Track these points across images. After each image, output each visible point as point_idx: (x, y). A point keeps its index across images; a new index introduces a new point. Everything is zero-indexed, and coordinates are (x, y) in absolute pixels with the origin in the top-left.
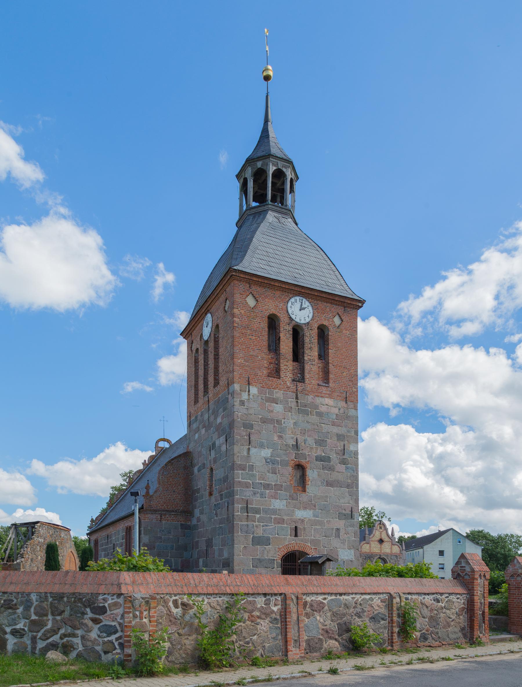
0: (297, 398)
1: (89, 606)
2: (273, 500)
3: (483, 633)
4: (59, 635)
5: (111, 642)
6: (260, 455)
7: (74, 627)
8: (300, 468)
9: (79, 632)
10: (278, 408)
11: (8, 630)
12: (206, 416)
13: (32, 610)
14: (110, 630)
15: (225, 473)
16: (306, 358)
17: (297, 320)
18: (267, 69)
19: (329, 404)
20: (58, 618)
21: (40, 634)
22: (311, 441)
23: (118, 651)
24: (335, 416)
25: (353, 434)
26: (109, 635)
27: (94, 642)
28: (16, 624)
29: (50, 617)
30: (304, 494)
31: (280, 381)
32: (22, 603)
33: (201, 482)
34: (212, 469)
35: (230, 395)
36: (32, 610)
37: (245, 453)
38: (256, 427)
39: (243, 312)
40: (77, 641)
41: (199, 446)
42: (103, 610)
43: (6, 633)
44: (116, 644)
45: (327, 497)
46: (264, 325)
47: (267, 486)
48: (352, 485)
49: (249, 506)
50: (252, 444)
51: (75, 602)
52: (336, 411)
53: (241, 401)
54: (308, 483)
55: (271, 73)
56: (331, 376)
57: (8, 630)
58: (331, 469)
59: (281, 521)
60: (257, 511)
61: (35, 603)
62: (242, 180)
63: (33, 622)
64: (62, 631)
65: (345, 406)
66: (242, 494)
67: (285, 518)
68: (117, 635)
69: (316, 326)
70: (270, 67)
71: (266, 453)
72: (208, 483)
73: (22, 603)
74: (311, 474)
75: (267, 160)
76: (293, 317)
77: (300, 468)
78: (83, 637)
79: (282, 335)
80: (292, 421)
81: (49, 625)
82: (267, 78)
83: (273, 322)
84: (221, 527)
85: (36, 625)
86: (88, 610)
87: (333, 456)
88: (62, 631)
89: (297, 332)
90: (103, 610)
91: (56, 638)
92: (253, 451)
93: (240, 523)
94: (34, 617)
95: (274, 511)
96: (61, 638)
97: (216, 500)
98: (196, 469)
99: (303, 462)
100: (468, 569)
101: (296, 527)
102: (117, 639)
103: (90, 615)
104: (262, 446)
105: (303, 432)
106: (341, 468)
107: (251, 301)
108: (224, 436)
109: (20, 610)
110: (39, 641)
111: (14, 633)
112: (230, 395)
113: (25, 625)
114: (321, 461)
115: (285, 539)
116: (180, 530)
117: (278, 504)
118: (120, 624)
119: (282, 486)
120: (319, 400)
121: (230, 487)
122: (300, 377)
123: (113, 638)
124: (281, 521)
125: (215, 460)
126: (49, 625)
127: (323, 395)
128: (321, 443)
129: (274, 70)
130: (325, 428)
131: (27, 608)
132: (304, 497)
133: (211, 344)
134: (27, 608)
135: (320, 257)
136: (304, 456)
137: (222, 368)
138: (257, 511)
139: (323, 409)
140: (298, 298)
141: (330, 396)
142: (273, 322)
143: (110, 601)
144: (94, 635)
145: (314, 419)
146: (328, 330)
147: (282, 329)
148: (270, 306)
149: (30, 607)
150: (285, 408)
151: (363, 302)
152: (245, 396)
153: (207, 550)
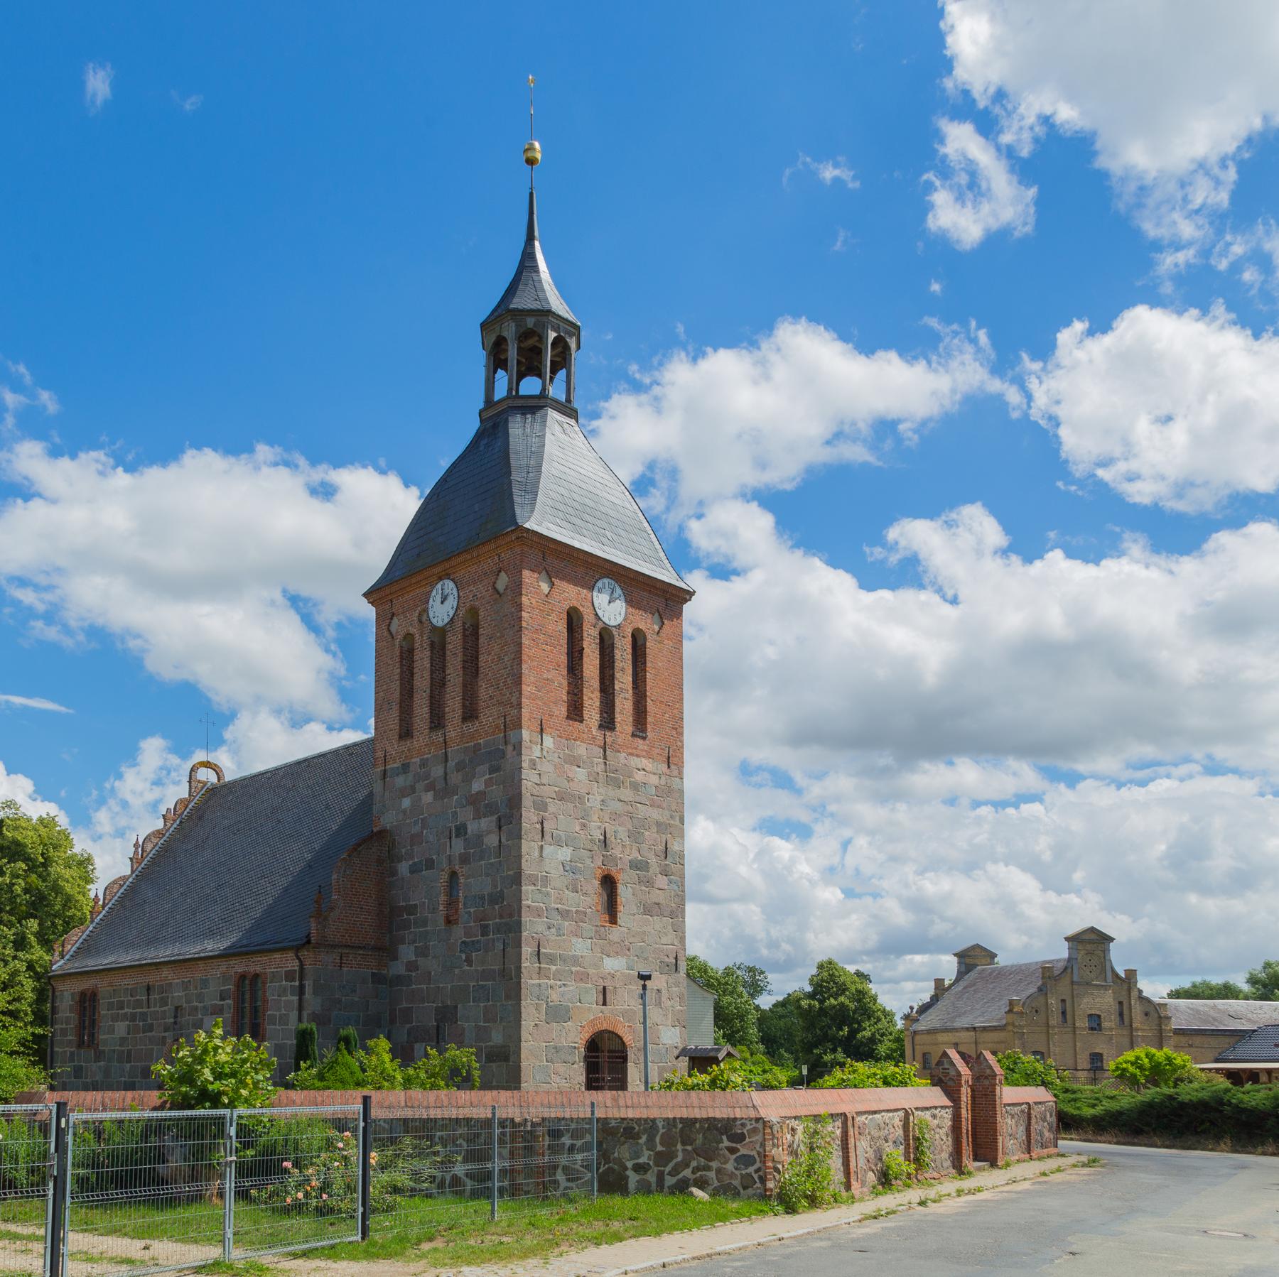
0: (605, 758)
1: (726, 1133)
2: (574, 940)
3: (969, 1163)
4: (690, 1170)
5: (749, 1175)
6: (559, 855)
7: (711, 1160)
8: (609, 883)
9: (714, 1164)
10: (580, 774)
11: (629, 1164)
12: (437, 771)
13: (658, 1139)
14: (747, 1161)
15: (496, 886)
16: (616, 687)
17: (606, 620)
18: (532, 148)
19: (645, 768)
20: (689, 1148)
21: (668, 1169)
22: (623, 834)
23: (758, 1185)
24: (653, 791)
25: (677, 823)
26: (747, 1166)
27: (732, 1175)
28: (638, 1157)
29: (679, 1147)
30: (614, 929)
31: (582, 726)
32: (645, 1131)
33: (424, 894)
34: (453, 875)
35: (510, 748)
36: (658, 1139)
37: (537, 854)
38: (551, 808)
39: (533, 601)
40: (712, 1174)
41: (415, 823)
42: (740, 1138)
43: (626, 1169)
44: (756, 1177)
45: (644, 933)
46: (562, 627)
47: (564, 914)
48: (677, 913)
49: (543, 950)
50: (547, 837)
51: (709, 1129)
52: (654, 780)
53: (531, 760)
54: (620, 908)
55: (539, 156)
56: (650, 719)
57: (629, 1164)
58: (649, 883)
59: (584, 977)
60: (552, 960)
61: (662, 1131)
62: (493, 338)
63: (658, 1154)
64: (694, 1164)
65: (668, 772)
66: (532, 927)
67: (591, 971)
68: (756, 1167)
69: (630, 630)
70: (537, 145)
71: (565, 854)
72: (442, 898)
73: (645, 1131)
74: (624, 893)
75: (544, 319)
76: (600, 613)
77: (609, 883)
78: (719, 1171)
79: (585, 644)
80: (599, 798)
81: (680, 1158)
82: (531, 162)
83: (574, 621)
84: (483, 986)
85: (663, 1158)
86: (724, 1137)
87: (653, 860)
88: (694, 1164)
89: (606, 640)
90: (740, 1138)
91: (687, 1173)
92: (548, 850)
93: (529, 981)
94: (659, 1148)
95: (576, 960)
96: (693, 1173)
97: (467, 934)
98: (403, 868)
99: (613, 872)
100: (952, 1073)
101: (604, 988)
102: (757, 1171)
103: (726, 1143)
104: (558, 843)
105: (615, 816)
106: (661, 881)
107: (545, 587)
108: (494, 818)
109: (644, 1138)
110: (667, 1177)
111: (639, 1168)
112: (510, 748)
113: (649, 1159)
114: (638, 869)
115: (589, 1009)
116: (370, 985)
117: (580, 947)
118: (759, 1153)
119: (585, 914)
120: (635, 762)
121: (511, 915)
122: (608, 723)
123: (751, 1170)
124: (584, 977)
125: (465, 859)
126: (680, 1158)
127: (639, 752)
128: (635, 836)
129: (543, 151)
130: (643, 811)
131: (651, 1140)
132: (615, 933)
133: (455, 642)
134: (651, 1140)
135: (628, 506)
136: (615, 860)
137: (484, 691)
138: (552, 960)
139: (639, 777)
140: (606, 581)
141: (649, 756)
142: (574, 621)
143: (749, 1127)
144: (730, 1166)
145: (627, 794)
146: (645, 639)
147: (585, 635)
148: (569, 594)
149: (655, 1136)
150: (589, 774)
151: (691, 594)
152: (536, 752)
153: (438, 1027)
